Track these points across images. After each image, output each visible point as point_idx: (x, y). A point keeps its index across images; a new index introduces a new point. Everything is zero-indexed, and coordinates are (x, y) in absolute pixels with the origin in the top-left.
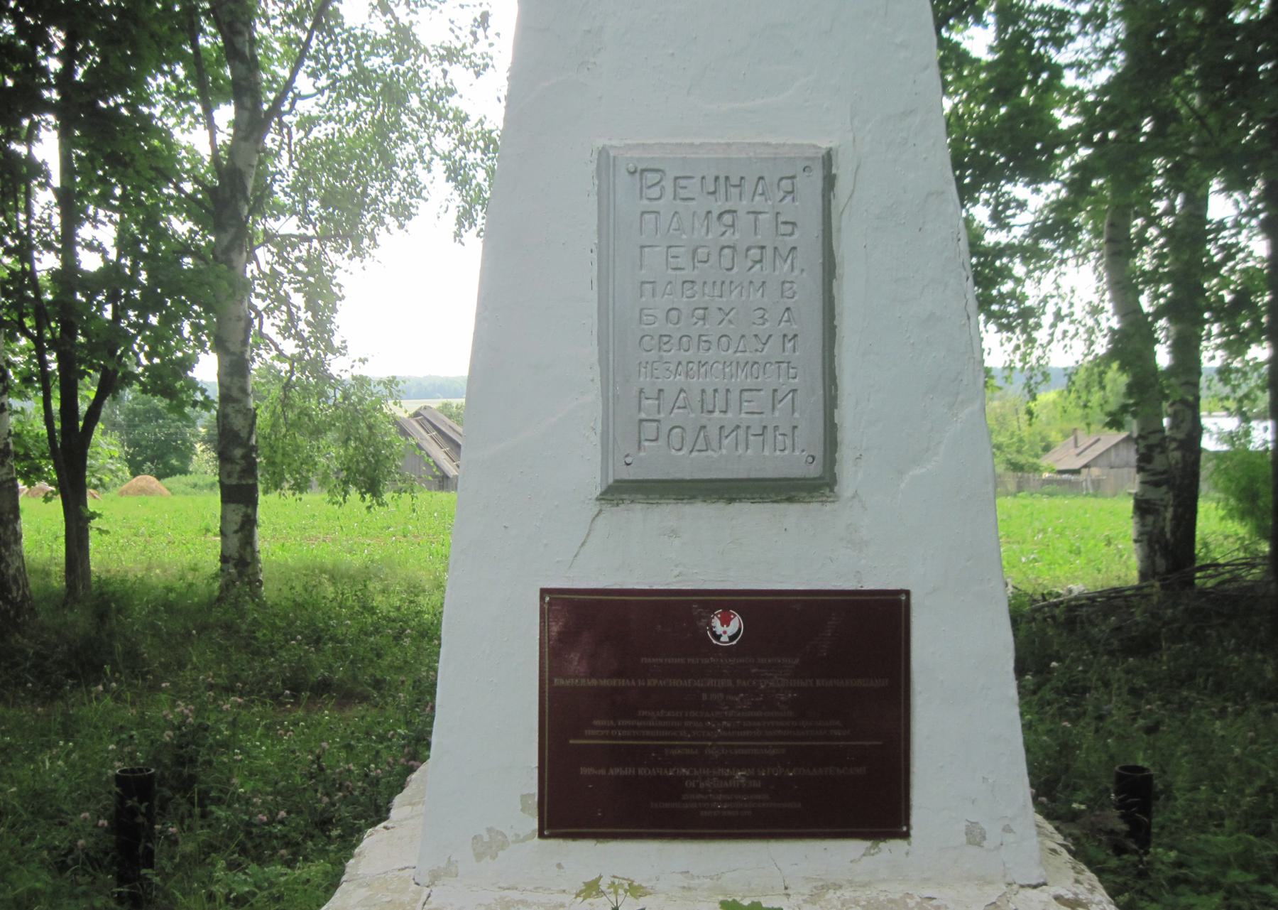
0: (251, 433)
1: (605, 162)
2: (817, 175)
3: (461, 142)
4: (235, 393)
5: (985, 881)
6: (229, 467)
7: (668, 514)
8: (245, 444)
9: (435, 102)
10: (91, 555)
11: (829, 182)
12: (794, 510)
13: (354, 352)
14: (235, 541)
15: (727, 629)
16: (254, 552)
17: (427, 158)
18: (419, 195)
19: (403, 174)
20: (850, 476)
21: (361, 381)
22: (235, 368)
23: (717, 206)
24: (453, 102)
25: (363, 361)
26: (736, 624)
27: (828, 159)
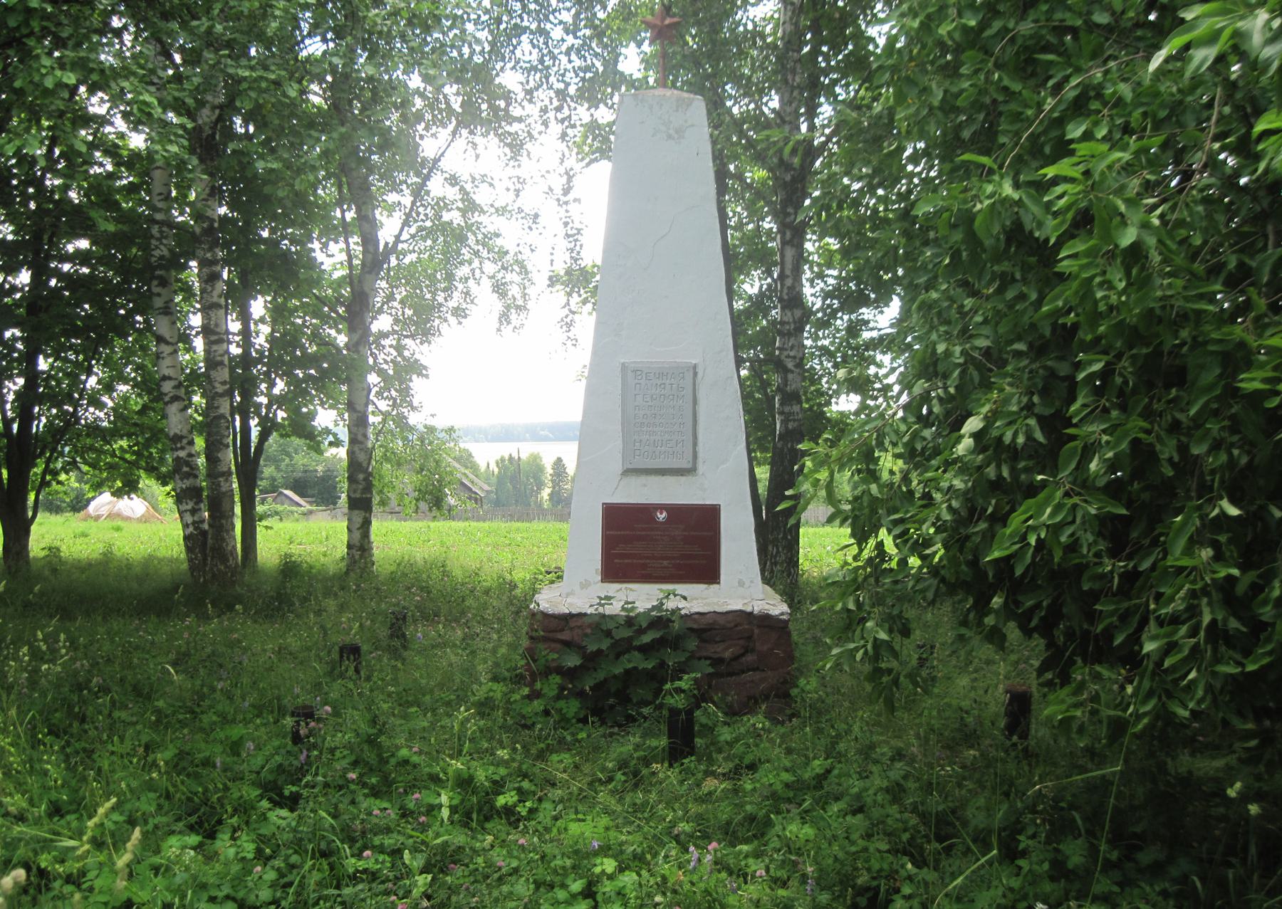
0: (369, 463)
1: (624, 367)
2: (691, 373)
3: (503, 268)
4: (360, 438)
5: (744, 598)
6: (354, 486)
7: (643, 479)
8: (365, 471)
9: (486, 240)
10: (259, 546)
11: (695, 374)
12: (683, 479)
13: (426, 411)
14: (357, 535)
15: (662, 516)
16: (369, 542)
17: (477, 276)
18: (472, 302)
19: (460, 287)
20: (701, 468)
21: (431, 430)
22: (358, 423)
23: (659, 382)
24: (499, 242)
25: (433, 416)
26: (664, 514)
27: (695, 367)
